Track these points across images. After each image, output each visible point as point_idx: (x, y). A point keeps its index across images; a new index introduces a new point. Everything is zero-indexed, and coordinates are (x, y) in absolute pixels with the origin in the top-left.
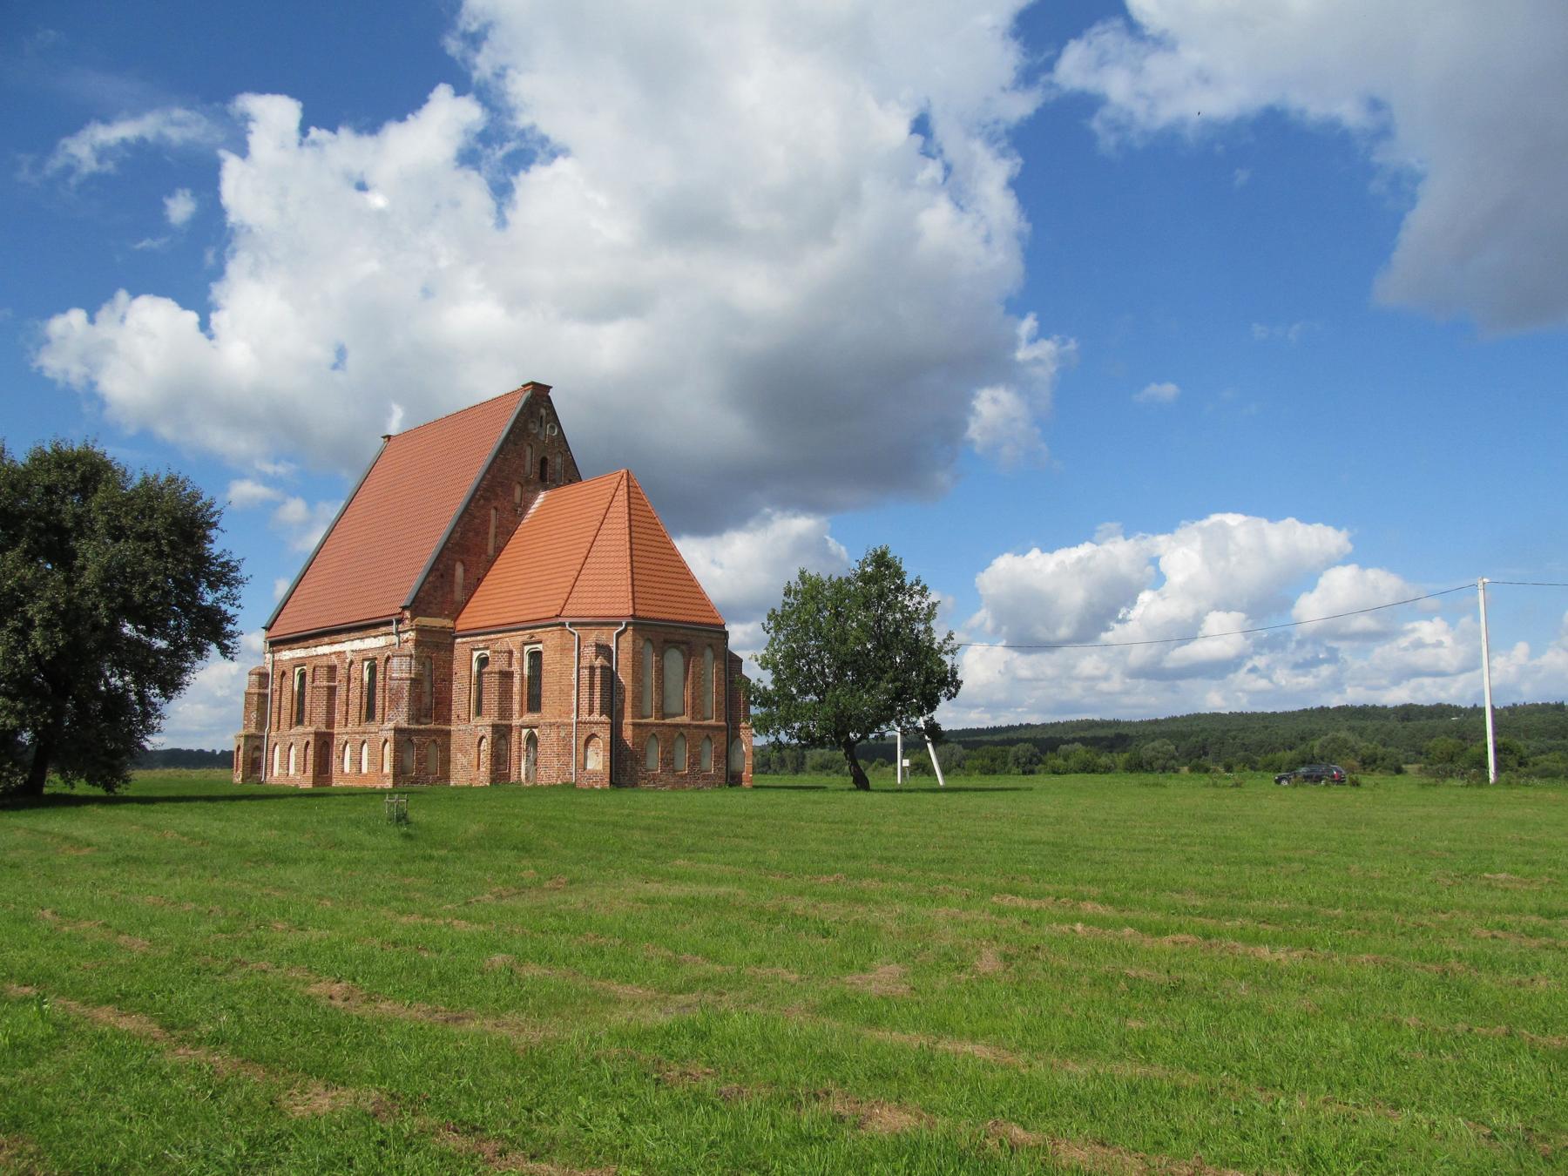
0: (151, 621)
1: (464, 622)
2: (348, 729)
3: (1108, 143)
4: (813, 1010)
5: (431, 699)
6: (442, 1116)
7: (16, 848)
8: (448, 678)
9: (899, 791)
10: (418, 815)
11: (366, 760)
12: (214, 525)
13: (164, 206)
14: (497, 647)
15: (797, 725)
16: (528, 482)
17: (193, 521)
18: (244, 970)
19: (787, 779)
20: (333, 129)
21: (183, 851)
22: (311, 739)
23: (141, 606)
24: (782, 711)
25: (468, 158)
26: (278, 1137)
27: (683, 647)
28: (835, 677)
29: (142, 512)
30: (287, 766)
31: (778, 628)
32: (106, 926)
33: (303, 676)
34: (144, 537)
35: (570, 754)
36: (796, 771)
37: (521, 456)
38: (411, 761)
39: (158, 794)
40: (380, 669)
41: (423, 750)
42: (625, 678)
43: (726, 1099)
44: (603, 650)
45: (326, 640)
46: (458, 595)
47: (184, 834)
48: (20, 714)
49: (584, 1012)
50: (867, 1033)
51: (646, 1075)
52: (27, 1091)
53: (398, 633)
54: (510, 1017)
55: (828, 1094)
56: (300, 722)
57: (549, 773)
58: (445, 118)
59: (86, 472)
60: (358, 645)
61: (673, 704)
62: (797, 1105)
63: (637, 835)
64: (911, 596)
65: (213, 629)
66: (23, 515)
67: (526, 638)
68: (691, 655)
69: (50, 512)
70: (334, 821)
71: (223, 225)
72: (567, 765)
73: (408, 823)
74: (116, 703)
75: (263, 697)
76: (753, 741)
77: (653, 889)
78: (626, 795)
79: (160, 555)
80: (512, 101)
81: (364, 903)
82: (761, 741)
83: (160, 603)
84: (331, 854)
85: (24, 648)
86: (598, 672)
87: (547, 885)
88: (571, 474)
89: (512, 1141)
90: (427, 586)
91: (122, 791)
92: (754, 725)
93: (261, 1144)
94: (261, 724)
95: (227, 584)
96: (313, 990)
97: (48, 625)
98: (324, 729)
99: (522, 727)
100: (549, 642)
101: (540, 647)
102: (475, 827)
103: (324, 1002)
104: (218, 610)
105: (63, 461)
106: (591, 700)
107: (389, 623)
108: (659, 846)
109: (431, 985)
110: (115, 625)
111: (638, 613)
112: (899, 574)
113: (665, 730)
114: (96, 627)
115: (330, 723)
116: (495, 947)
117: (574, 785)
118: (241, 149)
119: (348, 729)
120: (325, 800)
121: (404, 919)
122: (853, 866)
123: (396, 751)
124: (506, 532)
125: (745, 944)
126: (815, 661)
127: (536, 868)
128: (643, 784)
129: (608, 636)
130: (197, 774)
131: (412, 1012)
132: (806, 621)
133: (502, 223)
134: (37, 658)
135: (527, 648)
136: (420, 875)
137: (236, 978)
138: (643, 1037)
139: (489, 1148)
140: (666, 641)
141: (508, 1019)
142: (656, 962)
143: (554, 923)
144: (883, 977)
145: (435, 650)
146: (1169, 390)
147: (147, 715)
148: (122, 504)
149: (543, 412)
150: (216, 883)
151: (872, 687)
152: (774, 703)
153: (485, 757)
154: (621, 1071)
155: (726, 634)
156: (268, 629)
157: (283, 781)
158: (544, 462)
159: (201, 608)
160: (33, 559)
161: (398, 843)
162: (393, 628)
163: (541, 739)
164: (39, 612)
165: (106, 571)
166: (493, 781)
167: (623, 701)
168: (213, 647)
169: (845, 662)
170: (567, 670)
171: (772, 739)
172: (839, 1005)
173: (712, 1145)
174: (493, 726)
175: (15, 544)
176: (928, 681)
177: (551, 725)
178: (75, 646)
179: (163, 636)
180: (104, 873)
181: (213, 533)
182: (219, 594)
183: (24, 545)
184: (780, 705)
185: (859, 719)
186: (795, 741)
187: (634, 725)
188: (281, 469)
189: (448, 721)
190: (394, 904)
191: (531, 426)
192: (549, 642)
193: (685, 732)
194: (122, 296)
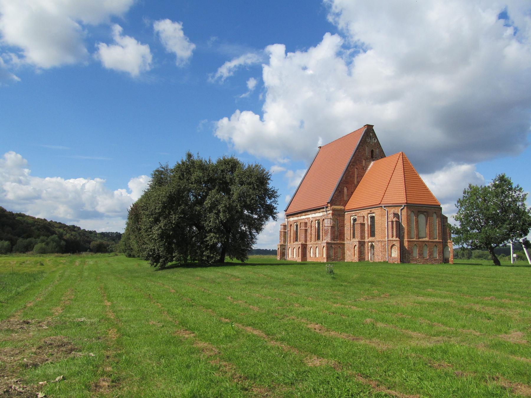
0: (252, 210)
1: (348, 207)
2: (312, 243)
4: (487, 346)
5: (338, 233)
6: (356, 371)
7: (219, 278)
8: (343, 226)
9: (513, 266)
10: (336, 271)
11: (318, 253)
12: (269, 179)
13: (247, 84)
14: (359, 215)
15: (470, 241)
16: (367, 159)
17: (263, 178)
18: (287, 318)
19: (466, 261)
20: (294, 52)
21: (265, 281)
22: (300, 246)
23: (249, 205)
24: (464, 236)
25: (339, 54)
26: (304, 372)
27: (425, 213)
28: (485, 223)
29: (248, 176)
30: (293, 255)
31: (461, 206)
32: (246, 302)
33: (297, 226)
34: (249, 184)
35: (386, 251)
36: (469, 258)
37: (364, 150)
38: (332, 253)
39: (256, 263)
40: (321, 223)
41: (336, 249)
42: (404, 225)
43: (457, 376)
44: (396, 215)
45: (304, 214)
46: (346, 198)
47: (265, 275)
48: (218, 238)
49: (400, 340)
50: (511, 357)
51: (426, 364)
52: (231, 350)
53: (326, 211)
54: (374, 340)
55: (498, 378)
56: (296, 240)
57: (378, 258)
58: (330, 43)
59: (232, 165)
60: (314, 215)
61: (422, 234)
62: (486, 381)
63: (412, 279)
64: (515, 192)
65: (270, 211)
66: (216, 179)
67: (369, 212)
68: (428, 216)
69: (223, 177)
70: (310, 272)
71: (264, 87)
73: (334, 274)
74: (243, 235)
75: (285, 233)
76: (452, 247)
77: (421, 299)
78: (406, 266)
79: (254, 189)
80: (351, 33)
81: (321, 299)
82: (456, 247)
83: (254, 204)
84: (310, 283)
85: (218, 218)
86: (395, 223)
87: (382, 296)
88: (382, 155)
89: (381, 382)
91: (246, 262)
92: (453, 241)
93: (300, 374)
94: (285, 241)
96: (309, 326)
97: (224, 212)
98: (304, 243)
100: (377, 213)
101: (374, 215)
102: (356, 276)
103: (313, 330)
105: (226, 162)
106: (392, 233)
107: (323, 208)
108: (421, 284)
109: (347, 327)
110: (242, 212)
111: (408, 202)
112: (510, 184)
113: (420, 243)
114: (237, 212)
115: (306, 241)
116: (366, 316)
117: (387, 262)
118: (268, 63)
119: (312, 243)
120: (306, 265)
121: (335, 305)
122: (497, 294)
123: (327, 250)
124: (361, 176)
125: (457, 320)
126: (476, 217)
127: (378, 290)
128: (412, 262)
129: (398, 211)
130: (266, 257)
131: (342, 336)
132: (472, 203)
133: (350, 74)
134: (221, 222)
135: (369, 215)
136: (339, 291)
137: (285, 321)
138: (423, 351)
139: (373, 384)
140: (419, 212)
141: (374, 341)
142: (424, 325)
143: (386, 309)
144: (515, 336)
145: (338, 216)
147: (252, 238)
148: (243, 174)
149: (371, 134)
150: (276, 291)
151: (500, 227)
152: (461, 233)
153: (357, 252)
154: (416, 362)
155: (441, 208)
156: (286, 211)
157: (292, 259)
158: (372, 151)
159: (267, 205)
160: (219, 192)
161: (331, 280)
162: (325, 210)
163: (375, 246)
165: (239, 195)
166: (359, 260)
167: (404, 233)
168: (271, 217)
169: (489, 218)
170: (384, 222)
171: (461, 246)
172: (497, 346)
173: (454, 391)
174: (359, 242)
175: (214, 188)
176: (524, 224)
177: (379, 241)
178: (232, 217)
179: (256, 214)
180: (244, 286)
181: (269, 181)
182: (271, 201)
183: (217, 188)
184: (463, 234)
185: (495, 239)
186: (470, 247)
187: (408, 241)
188: (286, 161)
189: (344, 240)
190: (331, 300)
192: (377, 213)
193: (427, 244)
194: (238, 111)
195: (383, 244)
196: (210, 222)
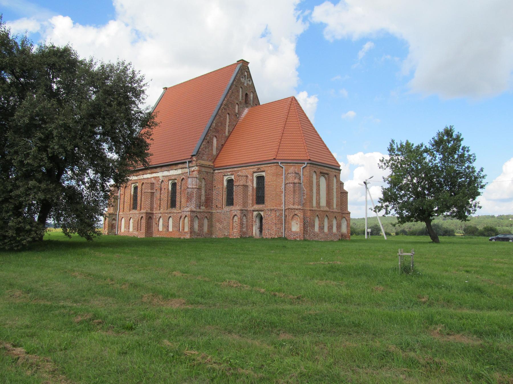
3: (327, 37)
22: (144, 215)
27: (326, 176)
35: (282, 224)
45: (149, 171)
56: (135, 207)
60: (166, 173)
67: (255, 170)
95: (149, 126)
98: (149, 211)
99: (254, 211)
101: (263, 174)
104: (142, 141)
115: (152, 209)
135: (255, 175)
140: (321, 173)
146: (351, 114)
149: (246, 74)
157: (126, 234)
162: (187, 165)
164: (56, 128)
177: (271, 210)
191: (242, 79)
195: (278, 214)
196: (27, 155)
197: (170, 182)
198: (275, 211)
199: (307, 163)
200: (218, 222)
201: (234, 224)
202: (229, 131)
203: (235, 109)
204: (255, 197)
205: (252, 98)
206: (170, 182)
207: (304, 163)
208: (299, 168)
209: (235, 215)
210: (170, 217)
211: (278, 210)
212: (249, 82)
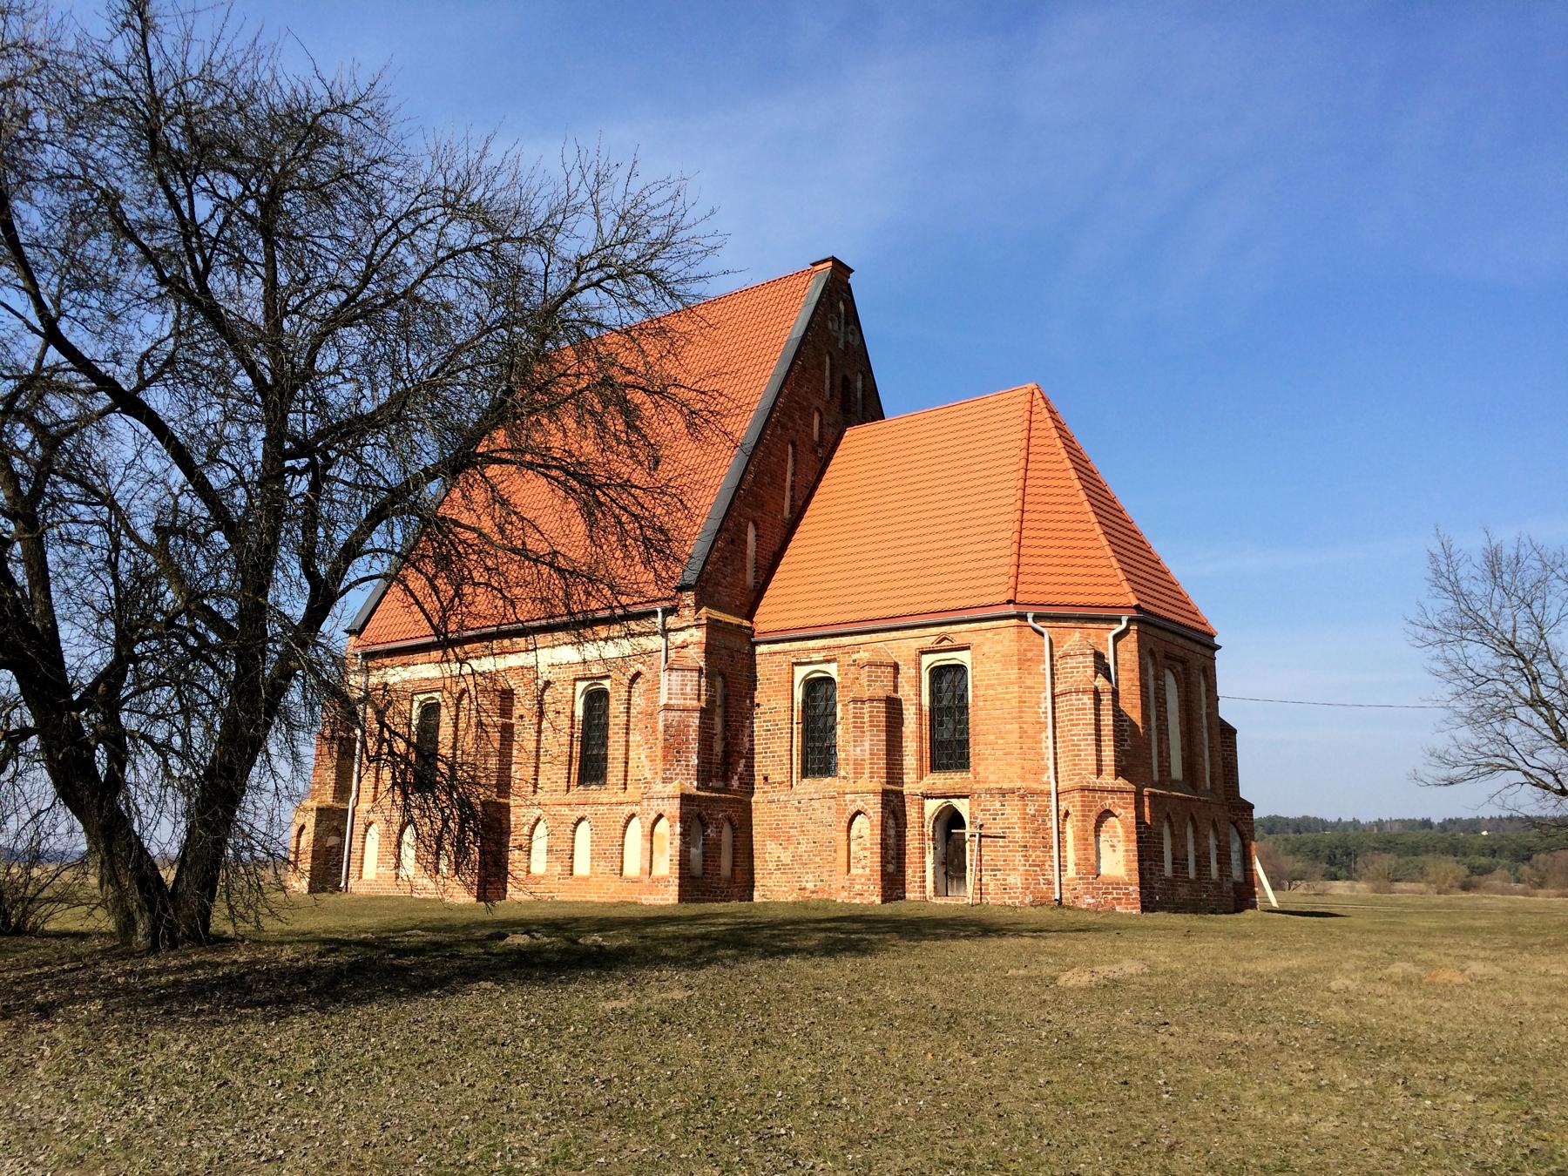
53: (665, 632)
67: (928, 643)
72: (1041, 865)
90: (716, 555)
101: (963, 657)
135: (927, 660)
157: (388, 889)
195: (1031, 810)
197: (581, 686)
198: (1022, 797)
199: (1130, 621)
200: (774, 837)
201: (853, 847)
202: (792, 506)
203: (810, 426)
204: (926, 745)
205: (859, 395)
206: (581, 686)
207: (1119, 621)
208: (1098, 636)
209: (859, 813)
210: (581, 819)
211: (1033, 793)
212: (850, 338)
